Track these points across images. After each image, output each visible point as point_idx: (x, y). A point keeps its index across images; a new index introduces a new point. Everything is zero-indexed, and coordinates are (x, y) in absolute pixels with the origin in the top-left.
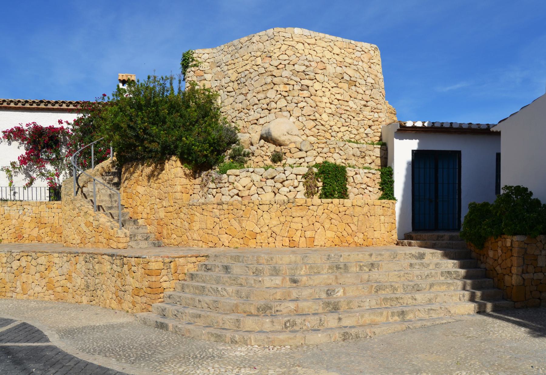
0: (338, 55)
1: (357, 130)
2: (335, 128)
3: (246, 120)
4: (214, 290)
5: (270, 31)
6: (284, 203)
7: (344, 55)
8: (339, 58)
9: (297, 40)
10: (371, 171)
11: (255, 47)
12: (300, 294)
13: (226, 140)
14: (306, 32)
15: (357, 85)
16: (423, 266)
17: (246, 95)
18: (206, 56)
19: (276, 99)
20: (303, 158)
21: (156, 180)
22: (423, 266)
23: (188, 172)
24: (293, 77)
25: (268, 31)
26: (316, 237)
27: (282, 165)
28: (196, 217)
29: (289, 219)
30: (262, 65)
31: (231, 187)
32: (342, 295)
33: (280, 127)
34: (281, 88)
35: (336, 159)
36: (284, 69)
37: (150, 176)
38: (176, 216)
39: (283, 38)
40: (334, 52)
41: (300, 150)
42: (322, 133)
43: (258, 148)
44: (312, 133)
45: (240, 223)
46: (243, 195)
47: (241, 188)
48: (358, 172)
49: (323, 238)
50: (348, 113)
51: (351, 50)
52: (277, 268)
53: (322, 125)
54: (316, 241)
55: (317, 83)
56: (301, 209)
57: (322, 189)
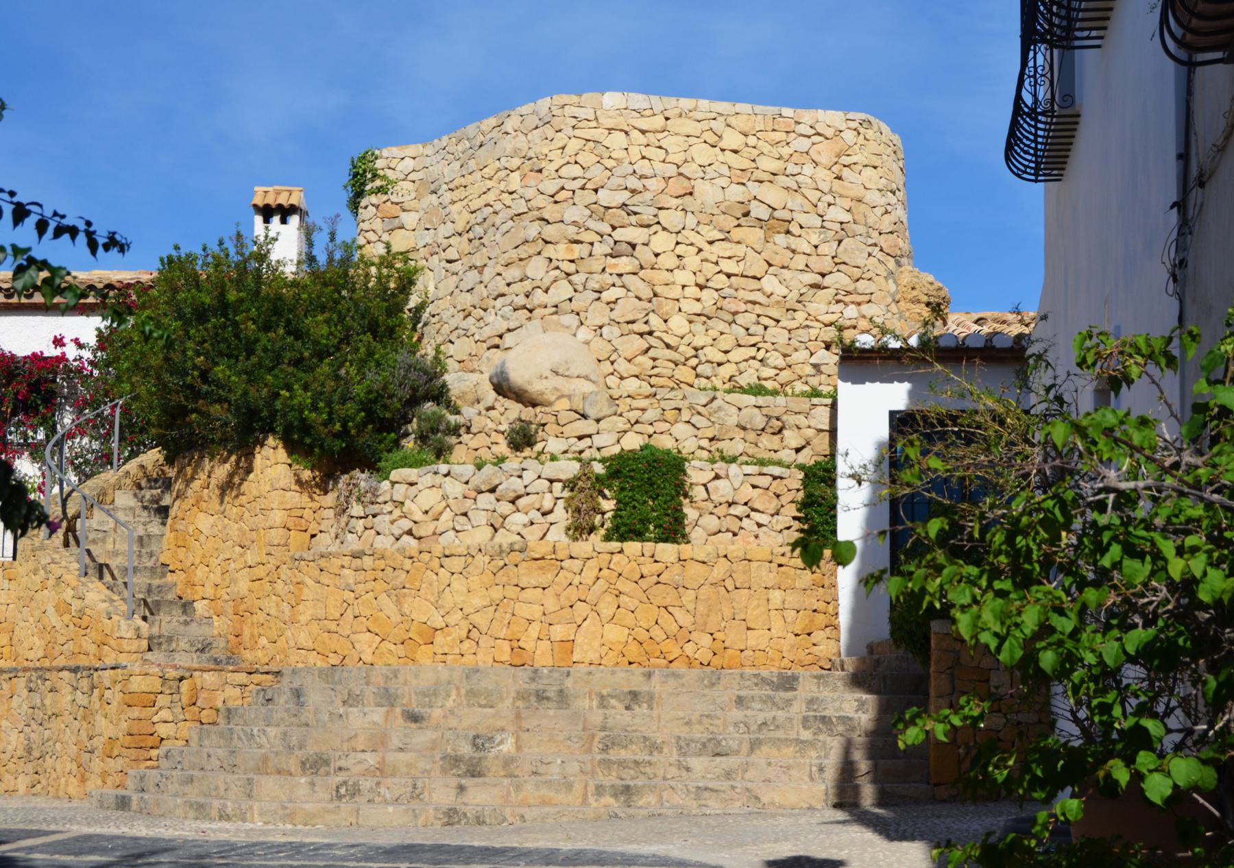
0: (736, 152)
1: (785, 356)
2: (714, 354)
3: (477, 337)
4: (246, 735)
5: (544, 104)
6: (502, 552)
7: (756, 152)
8: (738, 162)
9: (610, 123)
10: (765, 470)
11: (508, 144)
12: (408, 740)
13: (400, 393)
14: (639, 100)
15: (794, 228)
16: (774, 703)
17: (481, 269)
18: (409, 164)
19: (546, 282)
20: (590, 436)
21: (237, 497)
22: (774, 703)
23: (307, 475)
24: (591, 224)
25: (539, 102)
26: (579, 640)
27: (534, 455)
28: (306, 591)
29: (512, 592)
30: (521, 191)
31: (397, 513)
32: (513, 750)
33: (528, 361)
34: (560, 252)
35: (677, 437)
36: (571, 201)
37: (227, 487)
38: (268, 587)
39: (574, 122)
40: (722, 145)
41: (584, 416)
42: (665, 368)
43: (480, 414)
44: (635, 370)
45: (398, 602)
46: (422, 533)
47: (418, 516)
48: (722, 473)
49: (596, 644)
50: (758, 309)
51: (779, 136)
52: (392, 691)
53: (668, 346)
54: (577, 650)
55: (661, 234)
56: (541, 568)
57: (614, 517)
